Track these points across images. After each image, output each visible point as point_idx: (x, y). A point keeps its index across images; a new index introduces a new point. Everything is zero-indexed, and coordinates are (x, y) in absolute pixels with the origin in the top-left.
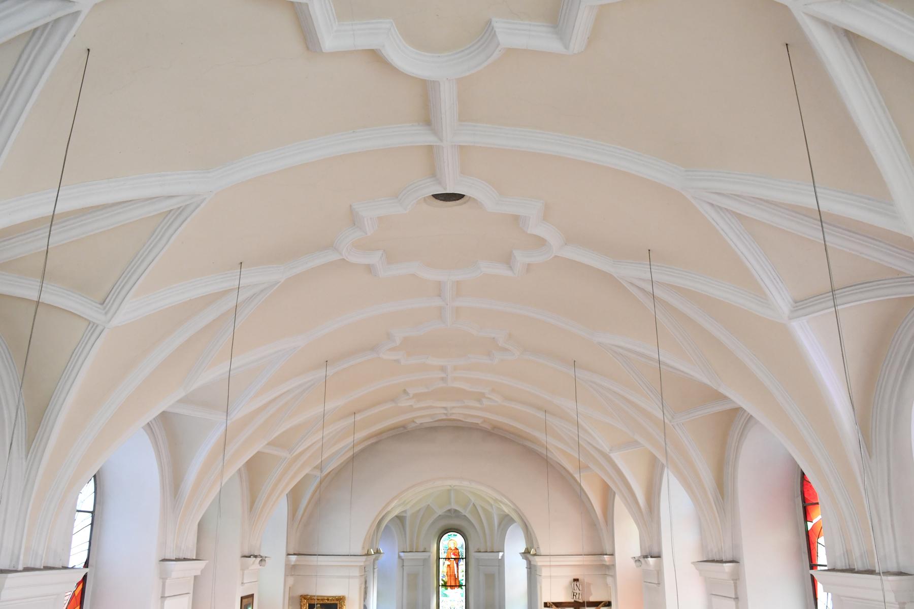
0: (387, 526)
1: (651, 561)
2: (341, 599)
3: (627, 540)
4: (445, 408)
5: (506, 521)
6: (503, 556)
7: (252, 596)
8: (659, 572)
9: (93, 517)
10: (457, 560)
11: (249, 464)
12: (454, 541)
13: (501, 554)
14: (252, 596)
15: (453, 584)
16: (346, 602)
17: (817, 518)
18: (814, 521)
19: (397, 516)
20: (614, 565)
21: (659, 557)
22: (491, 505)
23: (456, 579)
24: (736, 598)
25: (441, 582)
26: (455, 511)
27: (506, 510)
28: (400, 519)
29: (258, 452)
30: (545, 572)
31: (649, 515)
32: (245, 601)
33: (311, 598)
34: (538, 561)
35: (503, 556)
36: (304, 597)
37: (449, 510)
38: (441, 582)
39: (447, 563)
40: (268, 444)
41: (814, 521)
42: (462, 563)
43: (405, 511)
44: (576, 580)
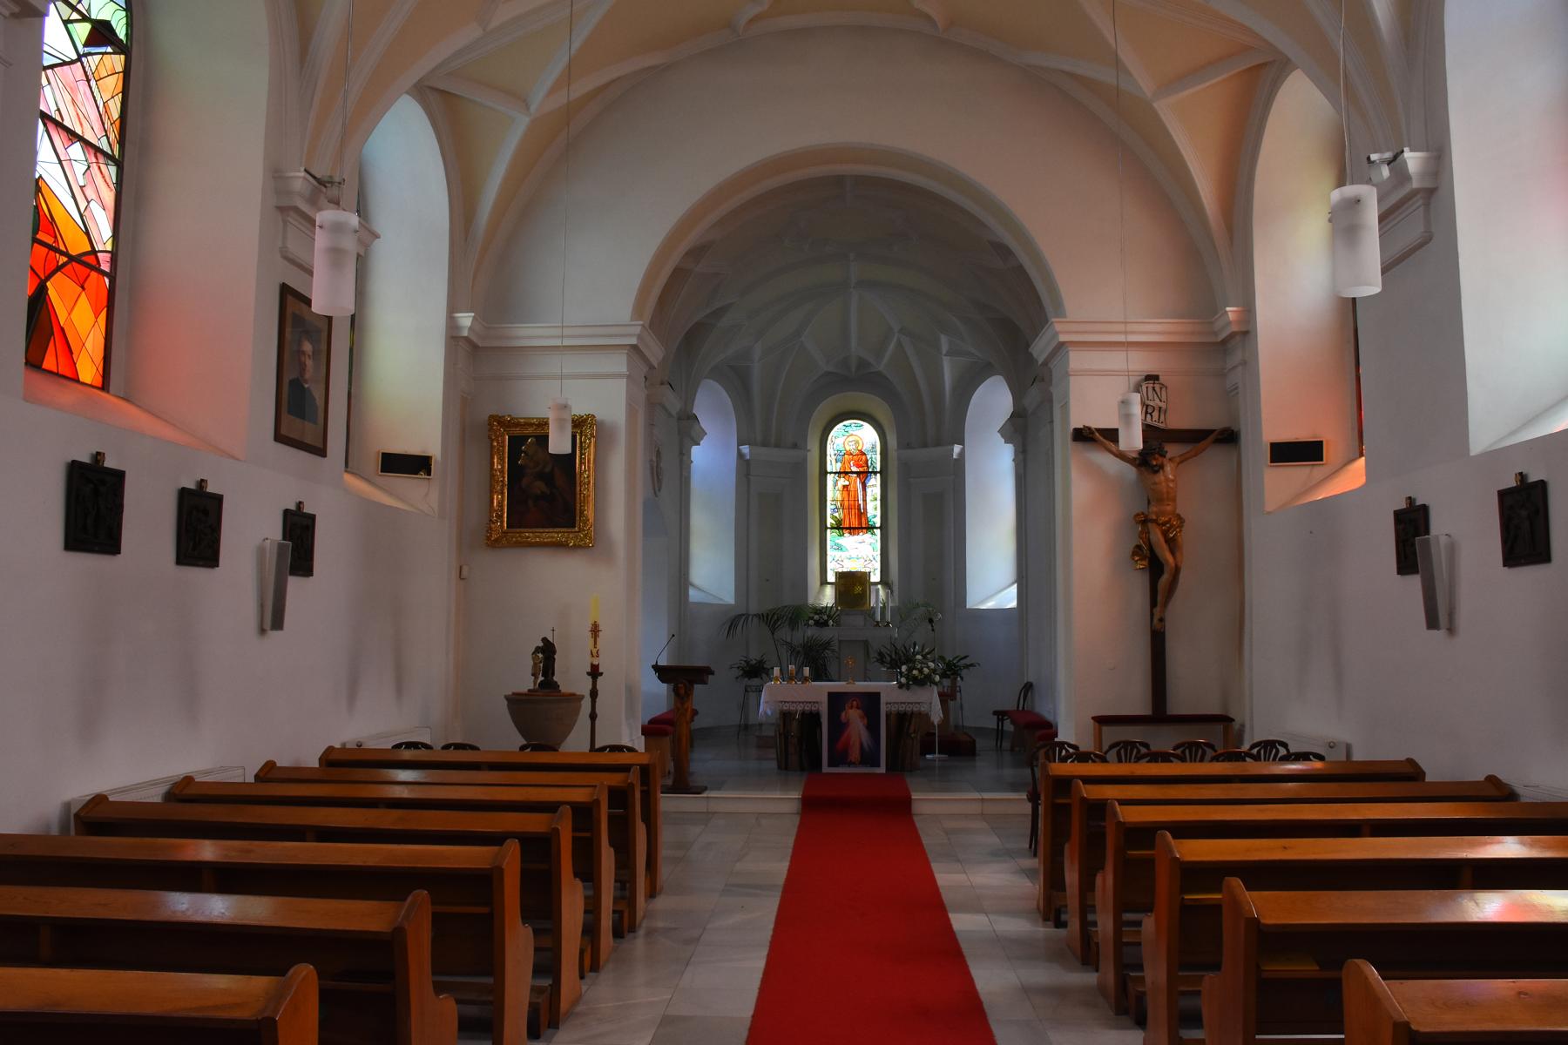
6: (962, 454)
10: (864, 475)
12: (855, 438)
13: (957, 449)
15: (855, 524)
23: (862, 514)
35: (962, 454)
36: (499, 422)
38: (830, 521)
39: (842, 482)
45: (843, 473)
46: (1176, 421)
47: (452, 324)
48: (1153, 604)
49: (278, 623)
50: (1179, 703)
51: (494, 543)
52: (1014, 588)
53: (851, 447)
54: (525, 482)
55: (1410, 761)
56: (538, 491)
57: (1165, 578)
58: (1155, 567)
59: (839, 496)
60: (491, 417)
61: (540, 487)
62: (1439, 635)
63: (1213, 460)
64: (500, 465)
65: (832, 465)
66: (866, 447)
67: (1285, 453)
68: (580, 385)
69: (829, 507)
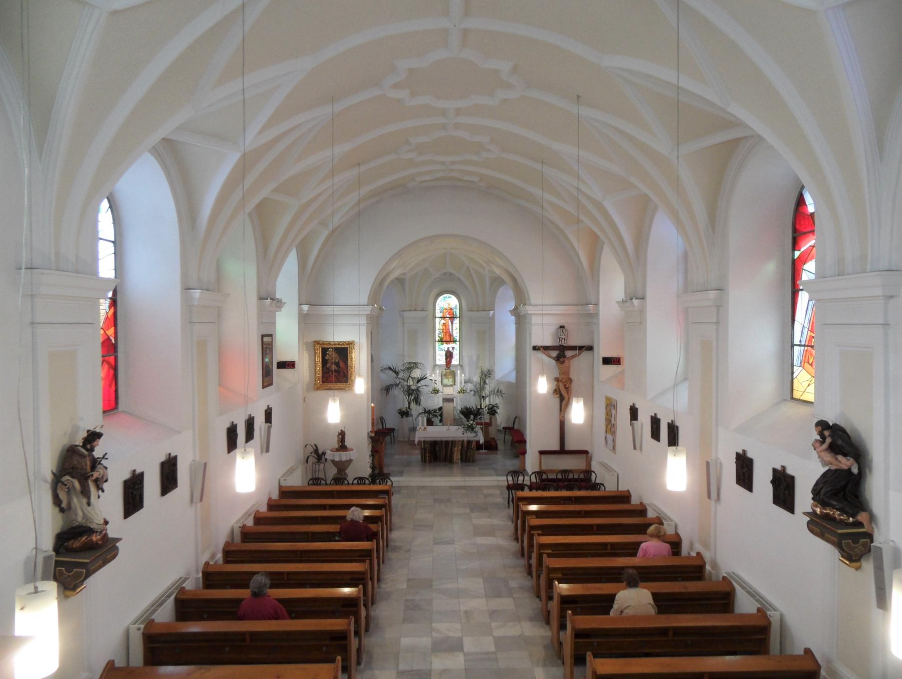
0: (387, 287)
1: (636, 302)
2: (351, 343)
3: (613, 288)
4: (443, 163)
5: (497, 282)
6: (493, 315)
7: (263, 387)
8: (642, 312)
9: (115, 246)
10: (452, 318)
11: (259, 206)
12: (448, 302)
13: (492, 313)
14: (263, 387)
15: (448, 339)
16: (356, 347)
17: (808, 243)
18: (802, 250)
19: (397, 279)
20: (597, 314)
21: (643, 298)
22: (484, 268)
23: (451, 336)
24: (718, 323)
25: (437, 338)
26: (451, 274)
27: (497, 271)
28: (400, 281)
29: (265, 199)
30: (535, 320)
31: (635, 263)
32: (265, 339)
33: (323, 343)
34: (529, 310)
35: (493, 315)
36: (317, 342)
37: (445, 274)
38: (437, 338)
39: (443, 321)
40: (272, 191)
41: (802, 250)
42: (457, 321)
43: (404, 274)
44: (562, 327)
45: (443, 318)
46: (572, 342)
47: (300, 310)
48: (561, 410)
49: (268, 451)
50: (570, 446)
51: (318, 389)
52: (514, 373)
53: (446, 306)
54: (328, 365)
55: (628, 491)
56: (334, 367)
57: (564, 402)
58: (562, 399)
59: (441, 327)
60: (315, 342)
61: (334, 367)
62: (638, 452)
63: (585, 355)
64: (319, 359)
65: (438, 314)
66: (453, 306)
67: (607, 361)
68: (349, 330)
69: (437, 332)
